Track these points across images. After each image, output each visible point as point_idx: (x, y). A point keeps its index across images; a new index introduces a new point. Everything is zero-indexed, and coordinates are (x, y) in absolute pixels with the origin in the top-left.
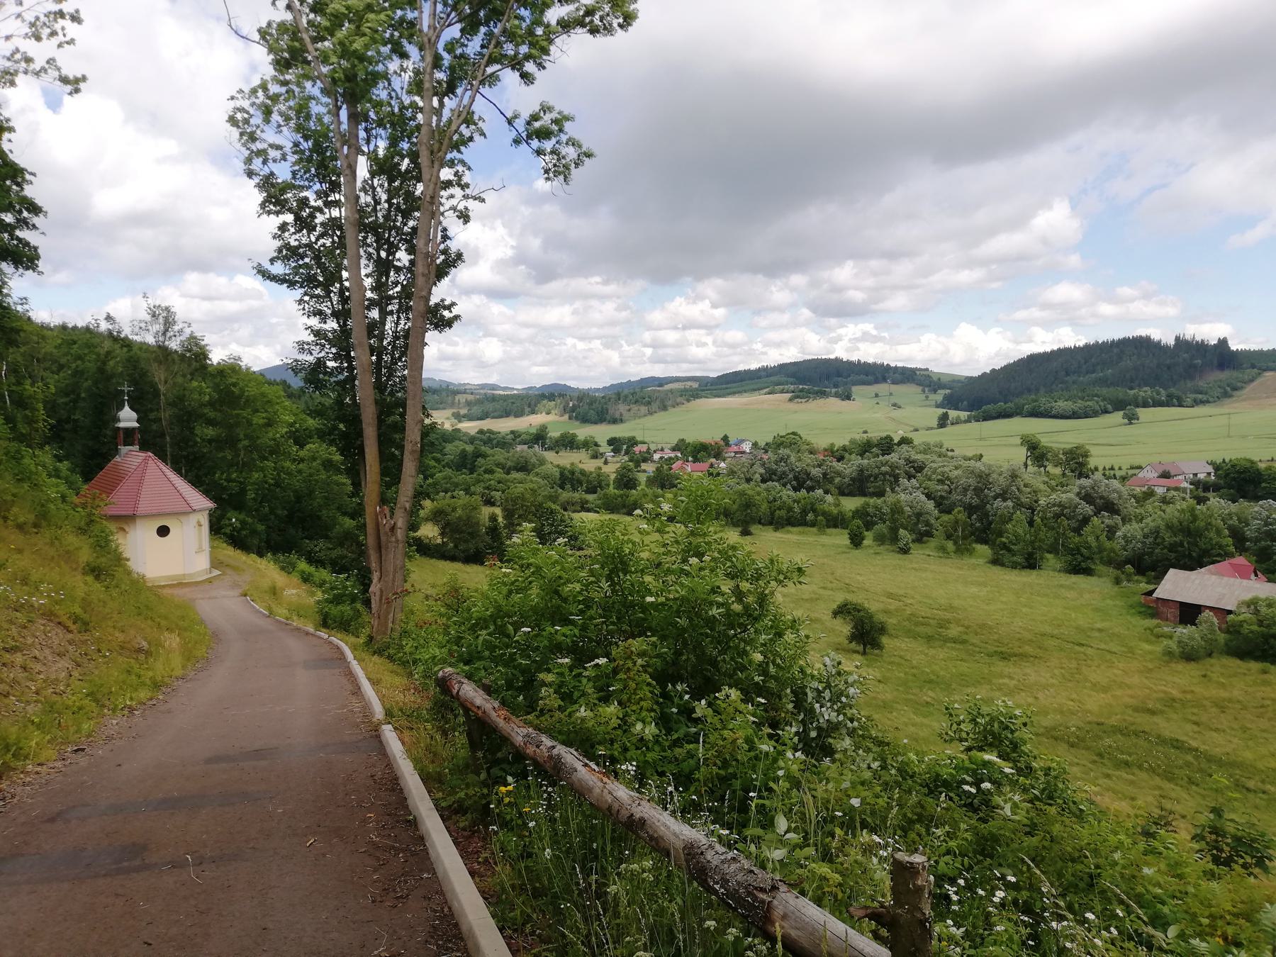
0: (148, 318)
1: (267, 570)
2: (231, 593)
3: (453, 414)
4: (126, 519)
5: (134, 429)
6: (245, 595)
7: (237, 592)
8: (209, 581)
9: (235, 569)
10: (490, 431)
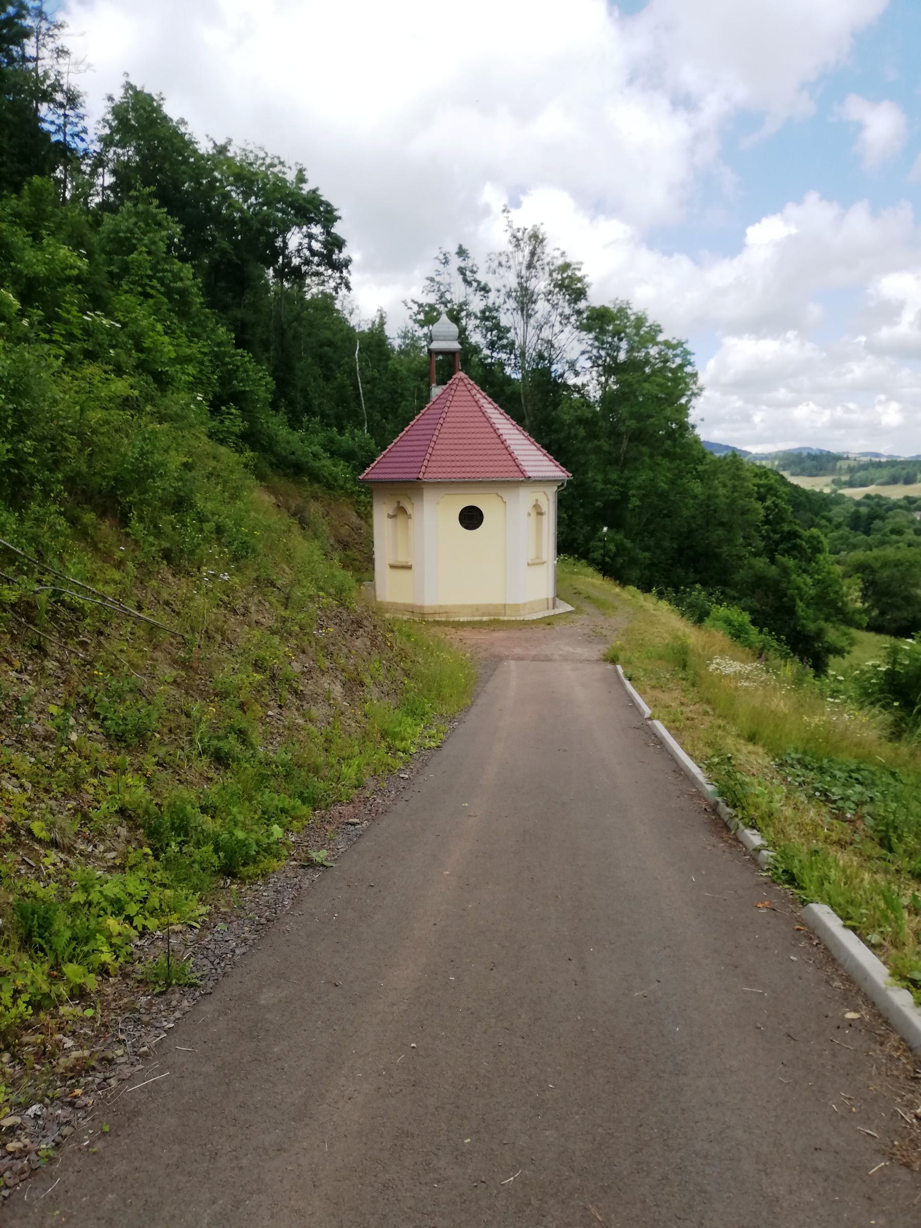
1: (661, 619)
3: (833, 481)
4: (407, 489)
6: (613, 660)
7: (594, 651)
8: (548, 622)
9: (600, 604)
10: (878, 497)
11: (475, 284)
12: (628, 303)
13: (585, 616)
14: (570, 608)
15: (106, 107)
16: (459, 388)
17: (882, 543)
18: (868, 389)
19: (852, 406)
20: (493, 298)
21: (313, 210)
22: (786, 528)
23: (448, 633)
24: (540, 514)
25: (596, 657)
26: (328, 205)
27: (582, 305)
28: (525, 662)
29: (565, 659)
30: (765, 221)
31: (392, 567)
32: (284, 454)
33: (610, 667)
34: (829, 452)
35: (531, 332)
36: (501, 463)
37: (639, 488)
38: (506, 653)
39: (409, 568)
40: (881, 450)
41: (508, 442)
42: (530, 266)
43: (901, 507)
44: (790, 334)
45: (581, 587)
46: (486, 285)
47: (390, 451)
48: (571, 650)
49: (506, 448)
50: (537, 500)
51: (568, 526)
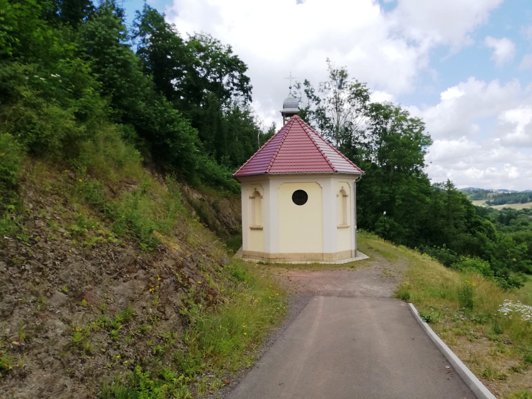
1: (427, 266)
4: (261, 179)
7: (386, 290)
8: (352, 266)
11: (313, 97)
12: (391, 103)
13: (377, 262)
14: (368, 257)
15: (135, 15)
16: (294, 123)
17: (518, 230)
18: (500, 161)
19: (493, 169)
20: (322, 104)
21: (235, 65)
22: (473, 220)
23: (281, 272)
24: (345, 196)
25: (389, 295)
26: (242, 62)
27: (367, 103)
28: (333, 298)
30: (449, 89)
31: (252, 229)
32: (210, 174)
33: (403, 304)
36: (318, 163)
37: (401, 194)
38: (319, 289)
39: (261, 229)
41: (328, 158)
44: (464, 137)
45: (372, 245)
46: (318, 98)
47: (252, 159)
48: (369, 287)
49: (322, 155)
50: (343, 187)
51: (363, 214)
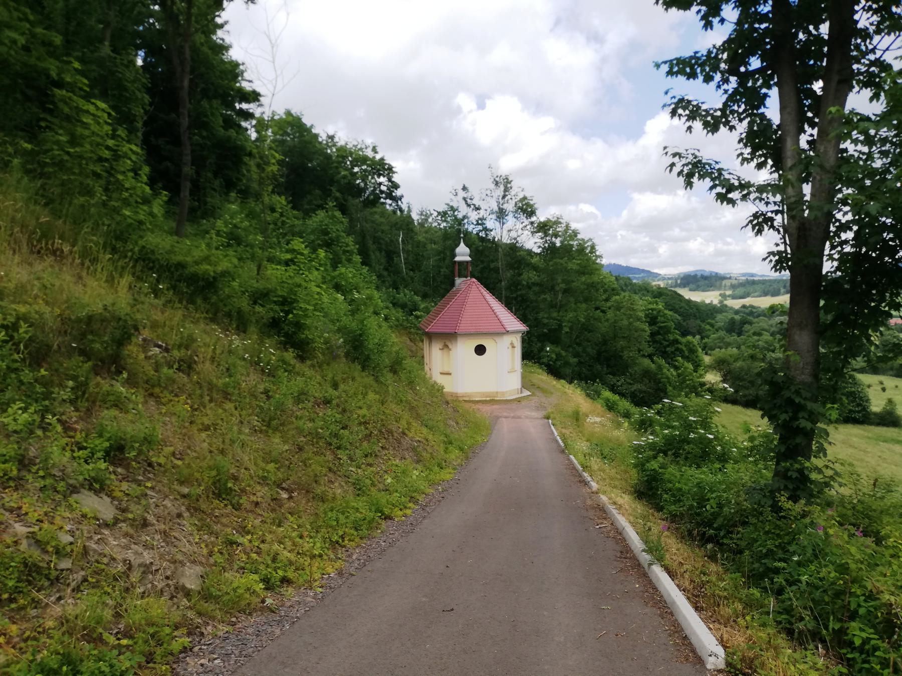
0: (493, 186)
1: (573, 396)
2: (534, 414)
3: (720, 295)
4: (448, 337)
5: (467, 262)
6: (548, 418)
8: (519, 400)
10: (752, 306)
14: (529, 393)
19: (729, 240)
22: (671, 337)
24: (513, 347)
27: (534, 219)
29: (527, 417)
34: (717, 274)
35: (505, 233)
40: (754, 271)
42: (504, 197)
43: (765, 315)
45: (535, 381)
51: (528, 343)
